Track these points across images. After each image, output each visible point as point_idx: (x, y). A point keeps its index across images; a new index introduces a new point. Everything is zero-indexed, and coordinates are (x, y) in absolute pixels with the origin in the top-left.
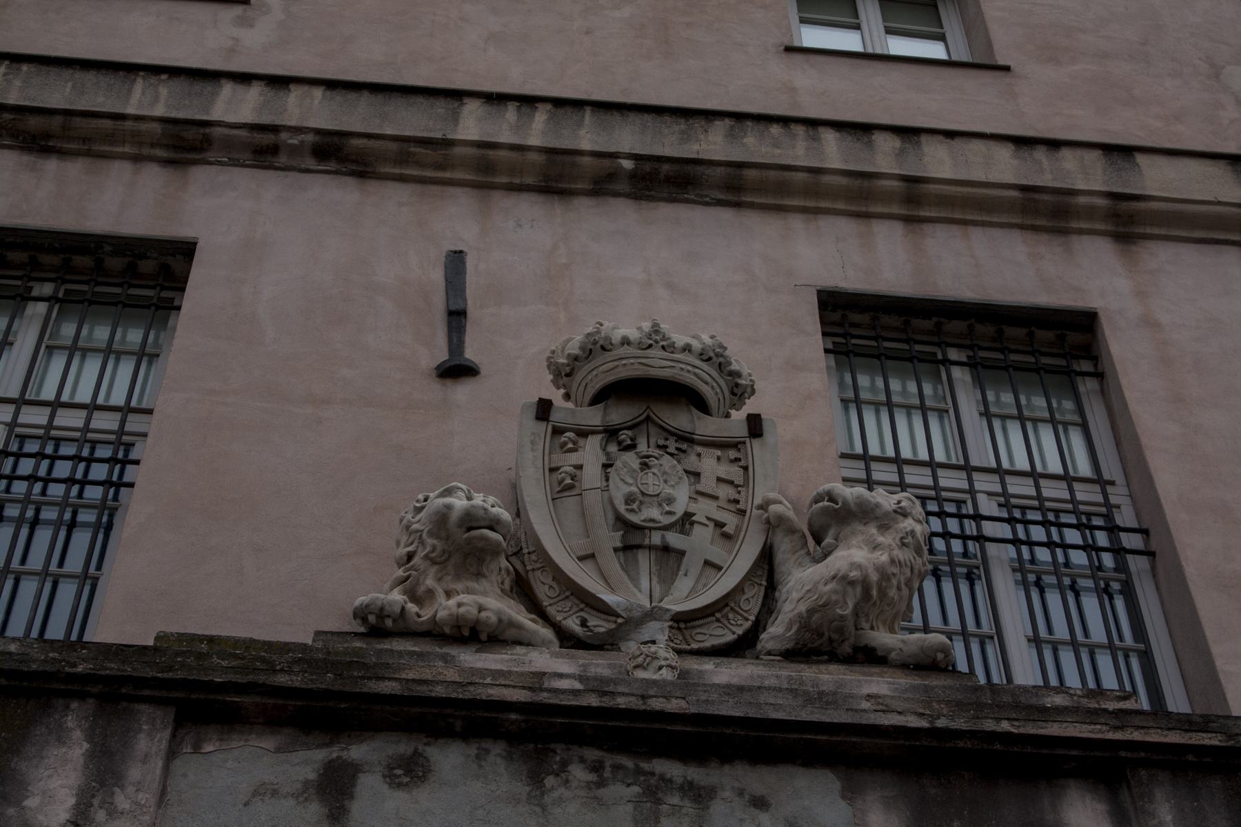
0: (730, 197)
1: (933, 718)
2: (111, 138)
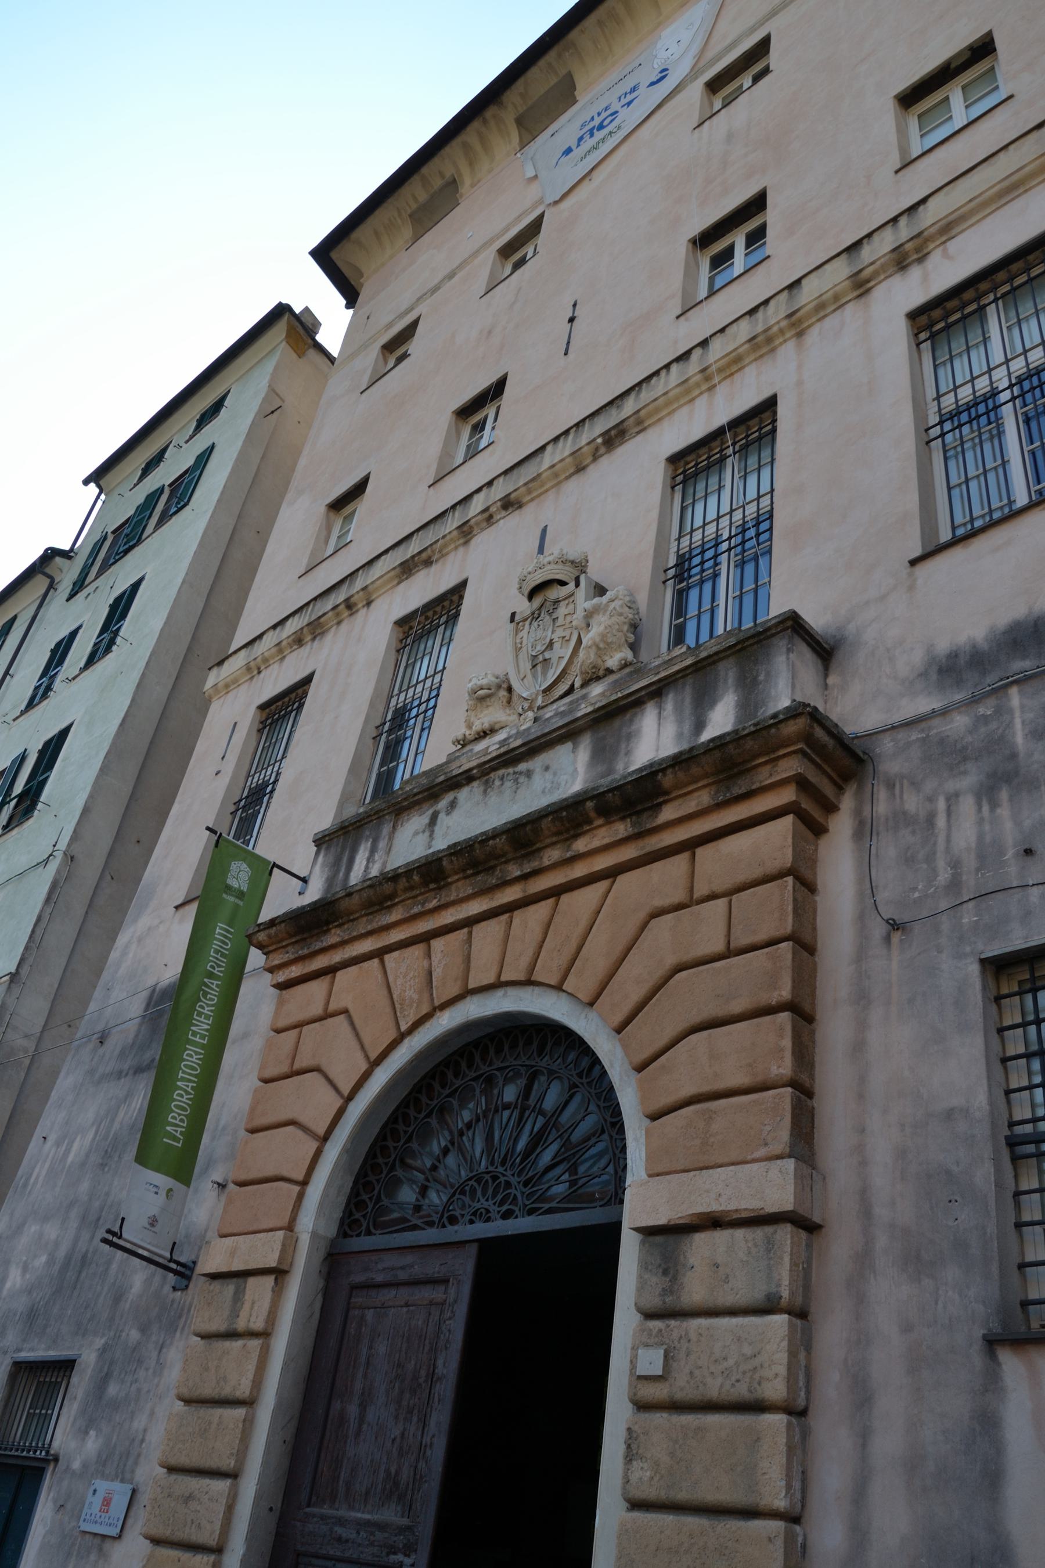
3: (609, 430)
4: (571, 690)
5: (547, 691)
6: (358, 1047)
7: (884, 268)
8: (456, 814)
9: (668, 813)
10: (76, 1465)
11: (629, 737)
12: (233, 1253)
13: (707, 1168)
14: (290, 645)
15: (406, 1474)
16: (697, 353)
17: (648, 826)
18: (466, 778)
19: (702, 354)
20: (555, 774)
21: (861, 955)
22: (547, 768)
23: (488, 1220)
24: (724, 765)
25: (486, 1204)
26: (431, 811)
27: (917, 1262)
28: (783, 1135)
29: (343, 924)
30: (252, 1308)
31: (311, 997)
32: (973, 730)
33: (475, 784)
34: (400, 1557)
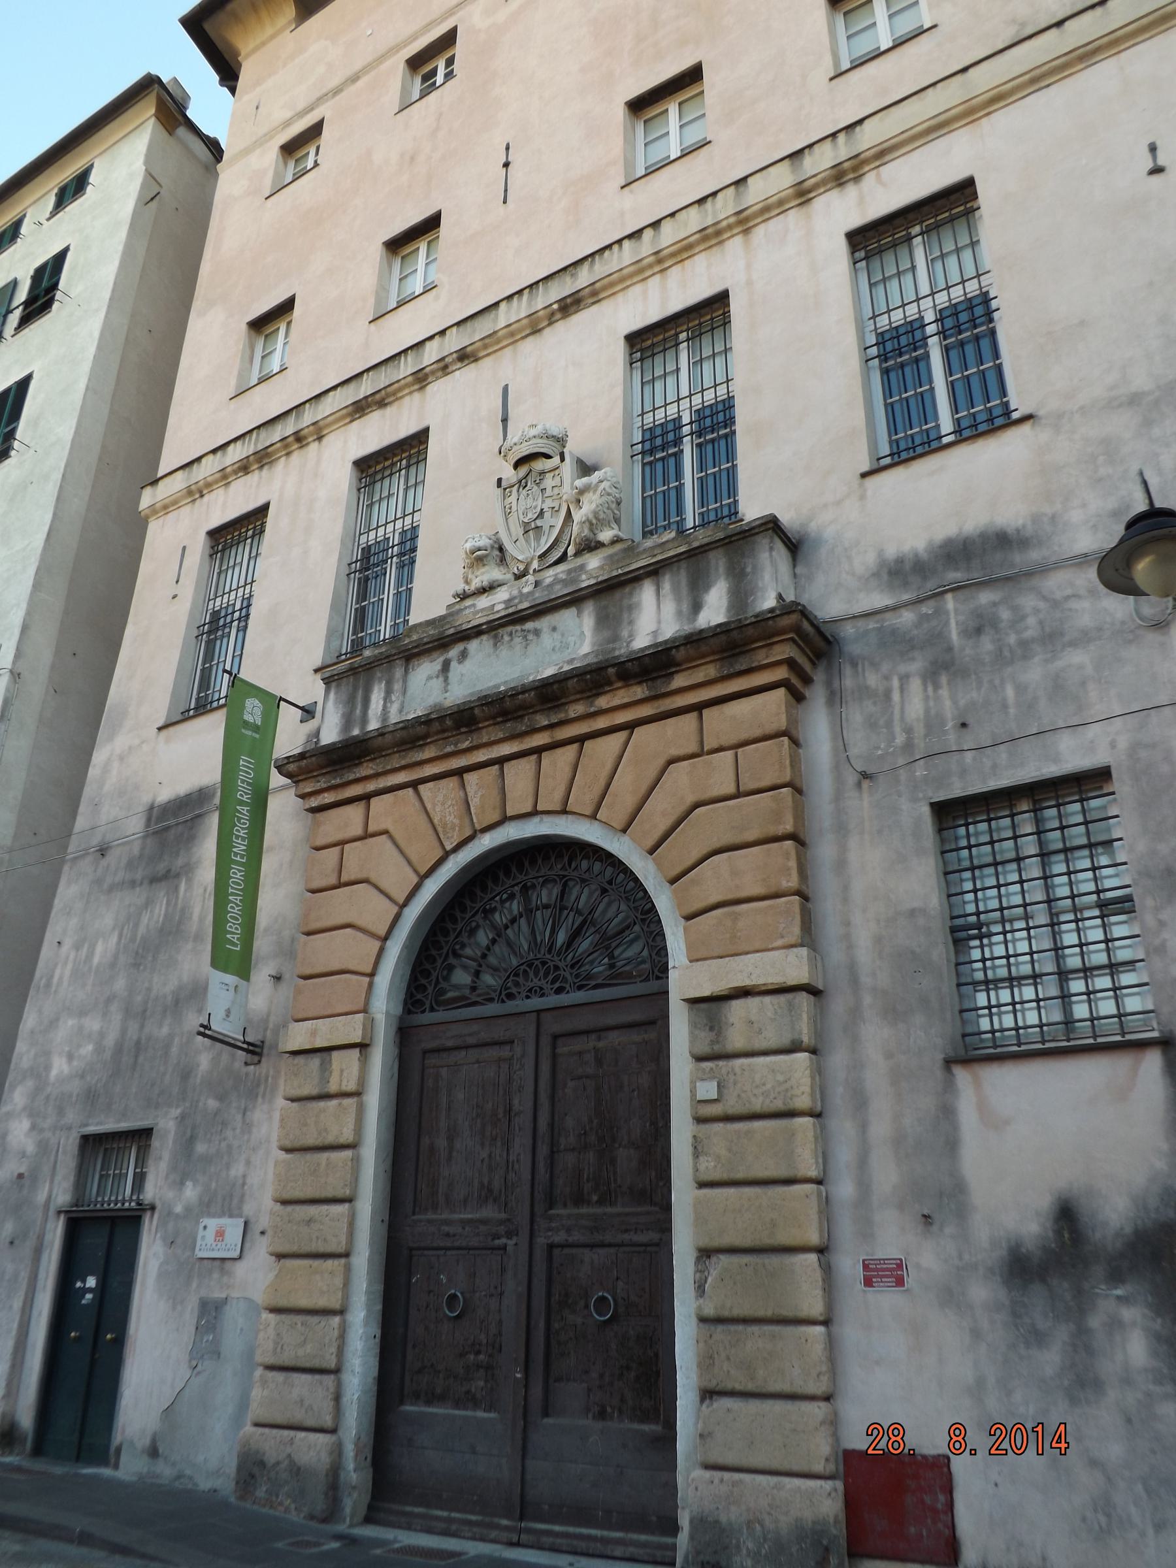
0: (595, 299)
1: (725, 529)
2: (400, 389)
3: (565, 298)
4: (563, 558)
5: (542, 556)
6: (405, 863)
7: (824, 182)
8: (468, 663)
9: (679, 681)
10: (178, 1209)
11: (630, 608)
12: (314, 1033)
13: (737, 955)
14: (235, 472)
15: (497, 1184)
16: (648, 234)
17: (663, 691)
18: (476, 632)
19: (654, 236)
20: (563, 635)
21: (838, 797)
22: (554, 629)
23: (542, 995)
24: (733, 645)
25: (539, 984)
26: (442, 659)
27: (893, 1012)
28: (796, 930)
29: (375, 759)
30: (341, 1075)
31: (350, 819)
32: (918, 625)
33: (484, 637)
34: (504, 1240)
